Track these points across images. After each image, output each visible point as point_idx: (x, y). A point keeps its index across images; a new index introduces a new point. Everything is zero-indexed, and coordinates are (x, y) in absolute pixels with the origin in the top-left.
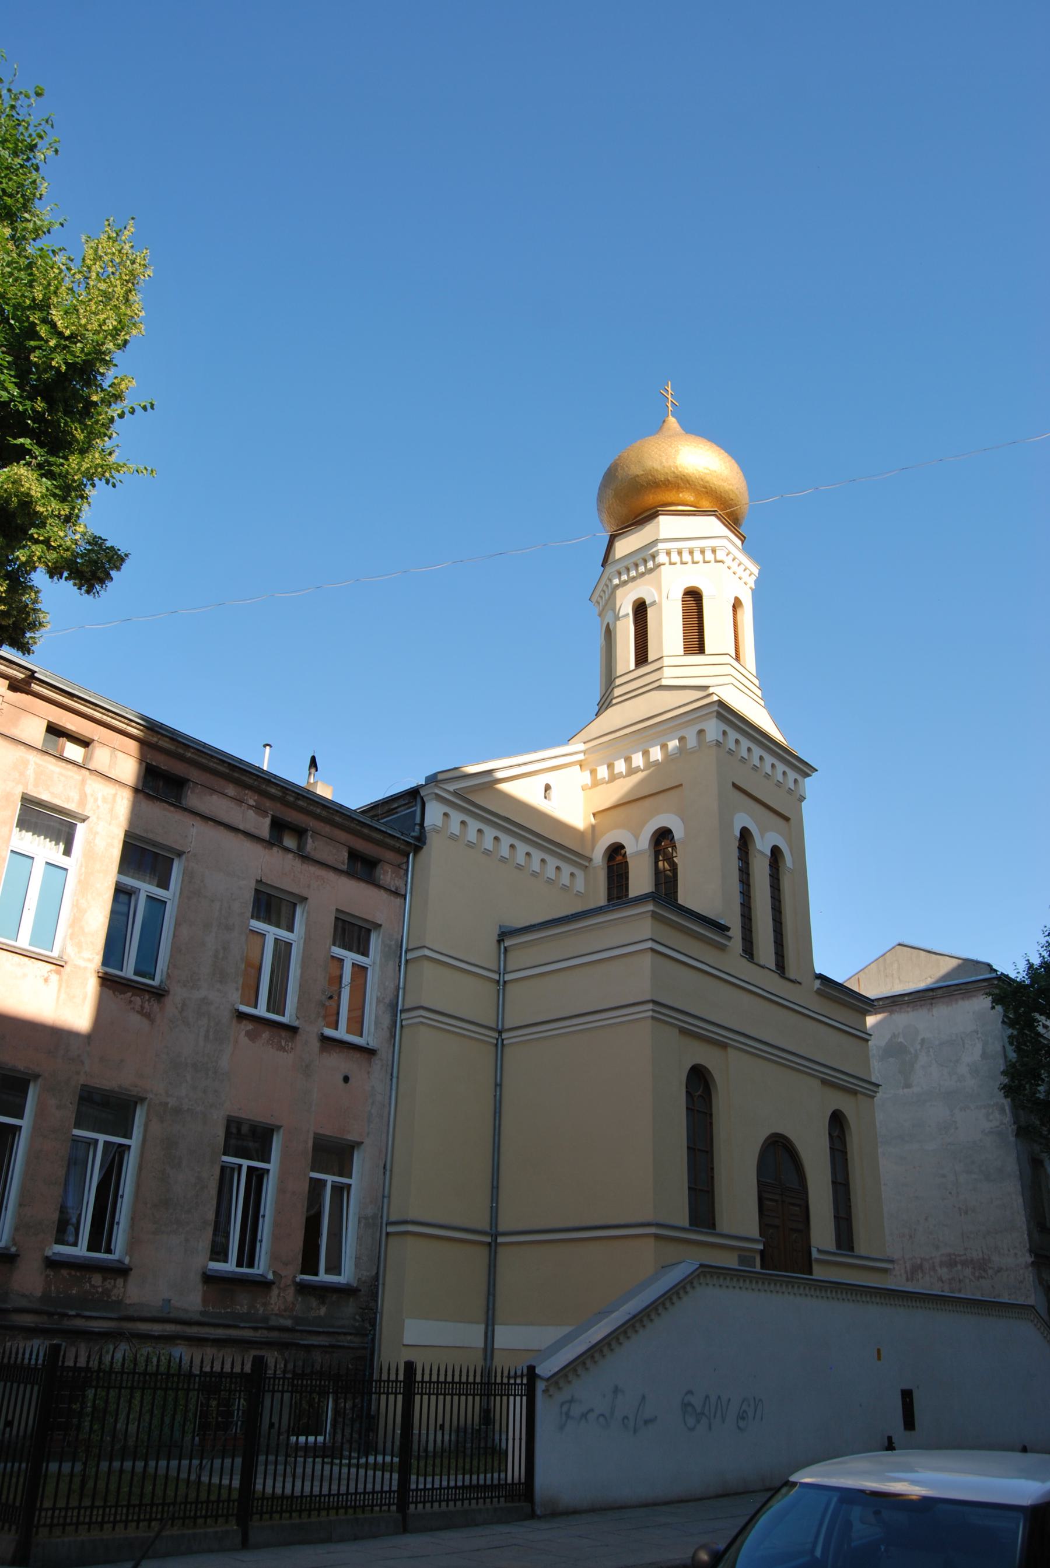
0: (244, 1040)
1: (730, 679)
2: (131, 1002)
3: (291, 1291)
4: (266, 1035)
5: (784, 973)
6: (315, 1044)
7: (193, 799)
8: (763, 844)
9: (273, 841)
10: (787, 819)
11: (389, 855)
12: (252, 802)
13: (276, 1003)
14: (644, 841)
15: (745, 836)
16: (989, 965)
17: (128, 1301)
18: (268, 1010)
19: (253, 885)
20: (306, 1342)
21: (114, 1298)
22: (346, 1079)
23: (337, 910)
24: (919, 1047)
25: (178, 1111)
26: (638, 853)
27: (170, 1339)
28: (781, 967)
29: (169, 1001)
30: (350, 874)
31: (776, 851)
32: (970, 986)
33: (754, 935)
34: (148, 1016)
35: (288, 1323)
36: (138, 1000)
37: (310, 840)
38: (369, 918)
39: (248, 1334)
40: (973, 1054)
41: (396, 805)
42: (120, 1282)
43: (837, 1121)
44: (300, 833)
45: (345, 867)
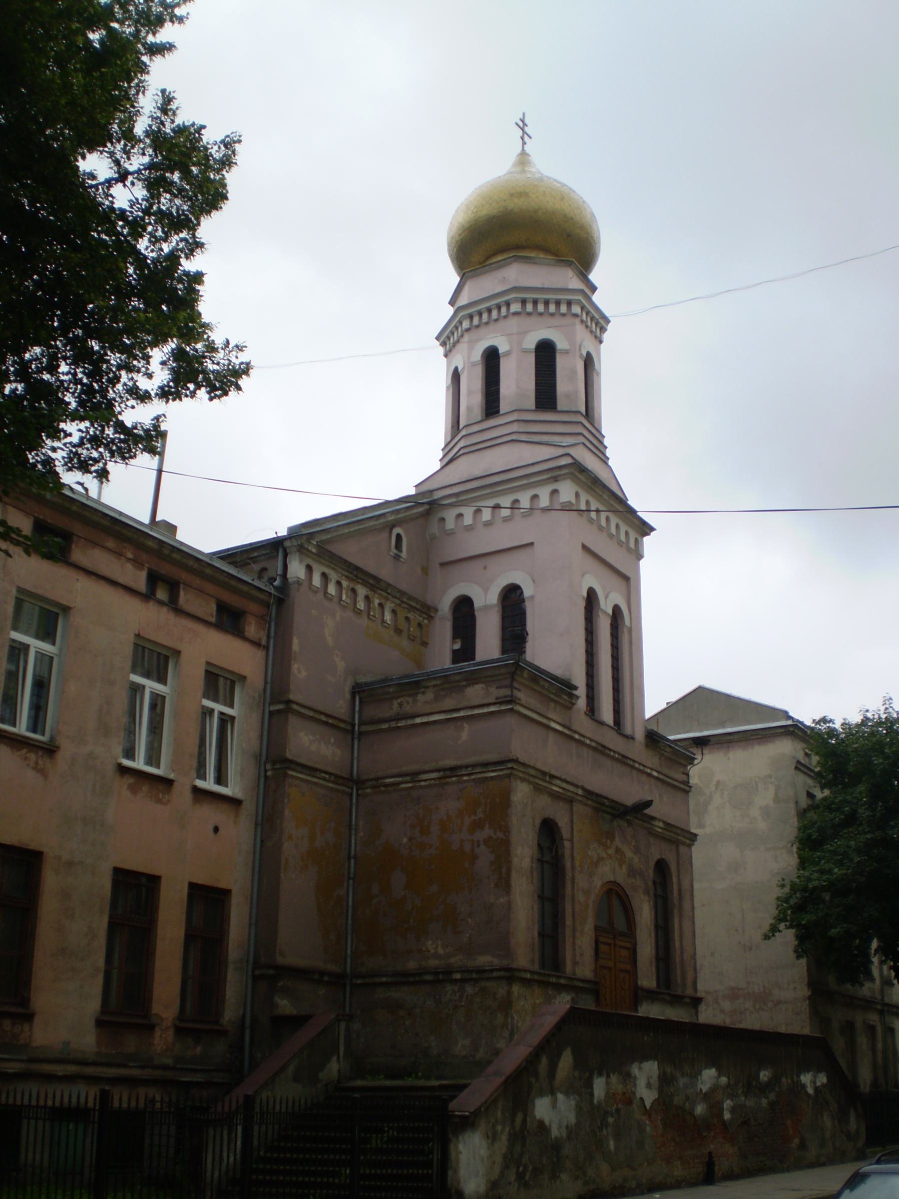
0: (126, 793)
1: (581, 439)
2: (26, 758)
3: (171, 1032)
4: (145, 788)
5: (593, 715)
6: (188, 795)
7: (78, 555)
8: (606, 605)
9: (148, 596)
10: (626, 579)
11: (252, 607)
12: (130, 555)
13: (153, 758)
14: (493, 597)
15: (591, 598)
16: (786, 712)
17: (34, 1044)
18: (28, 730)
19: (132, 638)
20: (186, 1079)
21: (22, 1042)
22: (216, 830)
23: (208, 663)
24: (713, 788)
25: (70, 864)
26: (486, 608)
27: (69, 1079)
28: (618, 721)
29: (60, 756)
30: (218, 626)
31: (617, 610)
32: (767, 732)
33: (595, 691)
34: (42, 772)
35: (169, 1061)
36: (32, 756)
37: (182, 593)
38: (236, 670)
39: (136, 1072)
40: (765, 798)
41: (256, 554)
42: (26, 1027)
43: (661, 867)
44: (173, 587)
45: (213, 620)
